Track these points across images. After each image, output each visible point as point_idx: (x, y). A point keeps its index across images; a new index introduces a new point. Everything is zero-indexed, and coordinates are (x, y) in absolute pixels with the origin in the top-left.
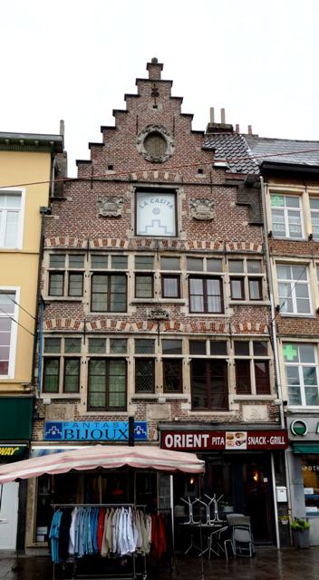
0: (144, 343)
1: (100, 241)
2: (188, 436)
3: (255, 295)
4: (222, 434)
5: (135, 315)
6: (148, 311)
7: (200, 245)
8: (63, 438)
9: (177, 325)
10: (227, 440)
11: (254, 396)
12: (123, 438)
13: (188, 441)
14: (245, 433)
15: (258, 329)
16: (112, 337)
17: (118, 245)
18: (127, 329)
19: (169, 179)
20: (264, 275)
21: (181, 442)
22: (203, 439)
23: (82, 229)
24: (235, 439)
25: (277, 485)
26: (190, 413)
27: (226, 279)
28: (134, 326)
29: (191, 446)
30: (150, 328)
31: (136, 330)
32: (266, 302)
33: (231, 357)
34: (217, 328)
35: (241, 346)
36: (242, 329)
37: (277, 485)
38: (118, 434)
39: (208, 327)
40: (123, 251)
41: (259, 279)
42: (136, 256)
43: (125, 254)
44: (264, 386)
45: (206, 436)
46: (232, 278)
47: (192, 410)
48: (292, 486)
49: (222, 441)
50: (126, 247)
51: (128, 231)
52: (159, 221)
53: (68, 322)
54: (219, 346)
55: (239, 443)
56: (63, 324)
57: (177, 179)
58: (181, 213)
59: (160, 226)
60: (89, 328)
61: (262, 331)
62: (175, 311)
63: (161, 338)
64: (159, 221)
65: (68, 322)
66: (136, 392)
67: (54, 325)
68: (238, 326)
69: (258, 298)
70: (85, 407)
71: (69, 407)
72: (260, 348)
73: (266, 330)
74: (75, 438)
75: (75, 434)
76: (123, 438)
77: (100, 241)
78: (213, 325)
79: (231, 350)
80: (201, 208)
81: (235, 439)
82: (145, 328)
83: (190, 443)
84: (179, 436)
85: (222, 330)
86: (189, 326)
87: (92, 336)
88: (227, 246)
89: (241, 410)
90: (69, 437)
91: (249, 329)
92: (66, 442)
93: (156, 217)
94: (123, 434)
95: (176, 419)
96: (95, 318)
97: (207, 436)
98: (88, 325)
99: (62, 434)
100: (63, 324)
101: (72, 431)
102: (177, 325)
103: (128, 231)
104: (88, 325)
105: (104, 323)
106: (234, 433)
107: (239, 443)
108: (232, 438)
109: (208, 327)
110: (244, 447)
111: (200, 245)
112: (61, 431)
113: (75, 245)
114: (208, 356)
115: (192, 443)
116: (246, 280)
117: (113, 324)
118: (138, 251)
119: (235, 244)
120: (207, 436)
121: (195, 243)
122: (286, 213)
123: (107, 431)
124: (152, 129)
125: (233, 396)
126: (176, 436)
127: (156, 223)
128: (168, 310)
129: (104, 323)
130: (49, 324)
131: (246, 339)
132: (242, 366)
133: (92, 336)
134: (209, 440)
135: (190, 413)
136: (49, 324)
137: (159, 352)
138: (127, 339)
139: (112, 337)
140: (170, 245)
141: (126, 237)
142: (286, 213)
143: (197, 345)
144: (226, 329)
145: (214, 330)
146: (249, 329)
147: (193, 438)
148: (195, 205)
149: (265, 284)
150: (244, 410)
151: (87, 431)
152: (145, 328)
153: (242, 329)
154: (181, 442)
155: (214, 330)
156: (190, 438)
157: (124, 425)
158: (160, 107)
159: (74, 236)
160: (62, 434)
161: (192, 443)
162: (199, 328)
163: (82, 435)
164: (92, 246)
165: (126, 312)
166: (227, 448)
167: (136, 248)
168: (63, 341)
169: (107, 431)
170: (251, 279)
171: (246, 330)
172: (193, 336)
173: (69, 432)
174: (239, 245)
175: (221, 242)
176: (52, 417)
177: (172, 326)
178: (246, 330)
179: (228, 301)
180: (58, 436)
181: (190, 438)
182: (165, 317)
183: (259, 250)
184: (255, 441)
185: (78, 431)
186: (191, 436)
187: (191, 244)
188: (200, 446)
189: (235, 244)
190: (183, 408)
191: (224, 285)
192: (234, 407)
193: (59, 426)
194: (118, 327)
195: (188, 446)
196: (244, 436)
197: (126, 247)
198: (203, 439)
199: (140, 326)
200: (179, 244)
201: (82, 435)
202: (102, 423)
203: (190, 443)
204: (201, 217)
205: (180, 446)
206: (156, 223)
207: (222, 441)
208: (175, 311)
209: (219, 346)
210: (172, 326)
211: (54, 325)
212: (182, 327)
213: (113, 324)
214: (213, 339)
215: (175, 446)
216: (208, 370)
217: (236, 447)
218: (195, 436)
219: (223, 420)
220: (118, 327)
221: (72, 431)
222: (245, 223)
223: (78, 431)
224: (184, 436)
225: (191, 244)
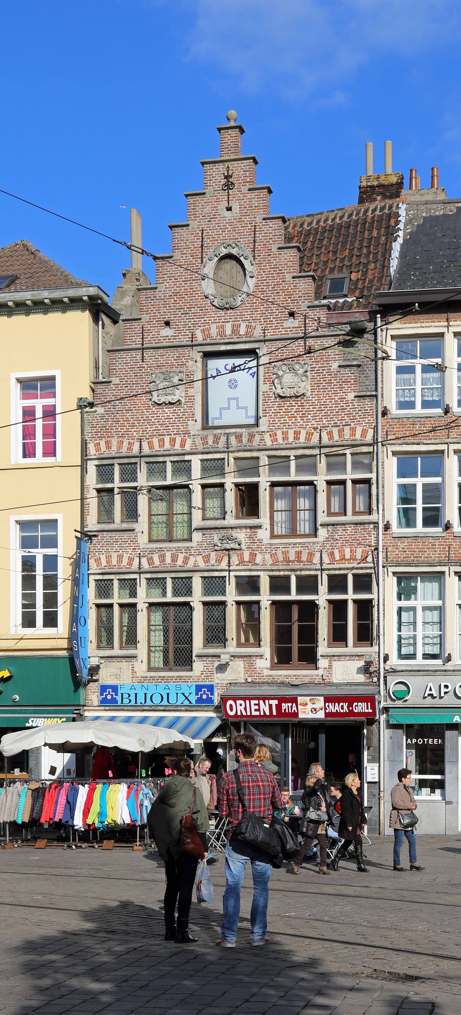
0: (214, 584)
1: (155, 441)
2: (253, 702)
3: (361, 505)
4: (294, 700)
5: (200, 544)
6: (216, 537)
7: (285, 438)
8: (120, 702)
9: (253, 556)
10: (300, 707)
11: (351, 648)
12: (186, 703)
13: (254, 707)
14: (322, 699)
15: (359, 557)
16: (173, 575)
17: (177, 446)
18: (190, 565)
19: (247, 333)
20: (373, 476)
21: (245, 709)
22: (271, 706)
23: (133, 426)
24: (310, 706)
25: (369, 761)
26: (267, 672)
27: (322, 486)
28: (200, 560)
29: (257, 713)
30: (219, 561)
31: (202, 564)
32: (373, 517)
33: (322, 597)
34: (304, 557)
35: (337, 583)
36: (337, 557)
37: (369, 761)
38: (181, 698)
39: (292, 557)
40: (184, 455)
41: (368, 481)
42: (202, 460)
43: (187, 458)
44: (366, 634)
45: (274, 703)
46: (330, 483)
47: (272, 668)
48: (387, 763)
49: (294, 708)
50: (188, 448)
51: (191, 423)
52: (237, 399)
53: (120, 557)
54: (308, 584)
55: (315, 710)
56: (114, 562)
57: (258, 333)
58: (263, 388)
59: (238, 408)
60: (145, 566)
61: (364, 559)
62: (250, 537)
63: (232, 574)
64: (237, 399)
65: (120, 557)
66: (205, 646)
67: (104, 563)
68: (332, 553)
69: (152, 665)
70: (145, 666)
71: (125, 665)
72: (364, 582)
73: (370, 559)
74: (133, 703)
75: (133, 698)
76: (186, 703)
77: (155, 441)
78: (299, 554)
79: (323, 587)
80: (288, 378)
81: (310, 706)
82: (213, 562)
83: (256, 710)
84: (242, 702)
85: (310, 560)
86: (268, 556)
87: (149, 576)
88: (324, 435)
89: (330, 666)
90: (126, 701)
91: (348, 556)
92: (122, 708)
93: (233, 393)
94: (187, 698)
95: (249, 680)
96: (152, 552)
97: (276, 702)
98: (144, 561)
99: (119, 698)
100: (114, 562)
101: (129, 695)
102: (253, 556)
103: (191, 423)
104: (144, 561)
105: (162, 558)
106: (308, 698)
107: (315, 710)
108: (306, 704)
109: (292, 557)
110: (321, 715)
111: (285, 438)
112: (117, 695)
113: (124, 450)
114: (294, 596)
115: (259, 710)
116: (349, 484)
117: (174, 559)
118: (203, 453)
119: (335, 431)
120: (276, 702)
121: (279, 433)
122: (419, 369)
123: (168, 694)
124: (224, 251)
125: (323, 648)
126: (239, 702)
127: (233, 403)
128: (241, 535)
129: (162, 558)
130: (98, 561)
131: (342, 572)
132: (339, 608)
133: (149, 576)
134: (279, 707)
135: (267, 672)
136: (98, 561)
137: (231, 595)
138: (191, 577)
139: (173, 575)
140: (245, 440)
141: (187, 433)
142: (419, 369)
143: (279, 584)
144: (316, 560)
145: (299, 561)
146: (348, 556)
147: (258, 705)
148: (280, 373)
149: (374, 488)
150: (333, 667)
151: (145, 694)
152: (213, 562)
153: (337, 557)
154: (245, 709)
155: (299, 561)
156: (255, 705)
157: (189, 689)
158: (236, 208)
159: (123, 436)
160: (119, 698)
161: (259, 710)
162: (281, 559)
163: (141, 699)
164: (146, 450)
165: (190, 540)
166: (301, 716)
167: (200, 448)
168: (169, 465)
169: (168, 694)
170: (355, 482)
171: (343, 558)
172: (273, 570)
173: (125, 696)
174: (341, 432)
175: (315, 429)
176: (106, 676)
177: (246, 558)
178: (343, 558)
179: (322, 518)
180: (114, 701)
181: (255, 705)
182: (237, 546)
183: (369, 438)
184: (334, 708)
185: (136, 694)
186: (257, 702)
187: (273, 436)
188: (268, 713)
189: (335, 431)
190: (258, 665)
191: (368, 447)
192: (322, 663)
193: (115, 688)
194: (180, 562)
195: (254, 713)
196: (320, 702)
197: (188, 448)
198: (271, 706)
199: (207, 559)
200: (257, 438)
201: (141, 699)
202: (163, 685)
203: (256, 710)
204: (288, 392)
205: (244, 714)
206: (233, 403)
207: (294, 708)
208: (250, 537)
209: (308, 584)
210: (246, 558)
211: (104, 563)
212: (259, 559)
213: (174, 559)
214: (298, 573)
215: (239, 714)
216: (295, 616)
217: (311, 716)
218: (261, 702)
219: (306, 680)
220: (180, 562)
221: (129, 695)
222: (351, 396)
223: (136, 694)
224: (247, 702)
225: (273, 436)
